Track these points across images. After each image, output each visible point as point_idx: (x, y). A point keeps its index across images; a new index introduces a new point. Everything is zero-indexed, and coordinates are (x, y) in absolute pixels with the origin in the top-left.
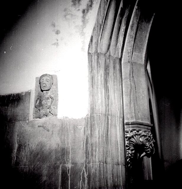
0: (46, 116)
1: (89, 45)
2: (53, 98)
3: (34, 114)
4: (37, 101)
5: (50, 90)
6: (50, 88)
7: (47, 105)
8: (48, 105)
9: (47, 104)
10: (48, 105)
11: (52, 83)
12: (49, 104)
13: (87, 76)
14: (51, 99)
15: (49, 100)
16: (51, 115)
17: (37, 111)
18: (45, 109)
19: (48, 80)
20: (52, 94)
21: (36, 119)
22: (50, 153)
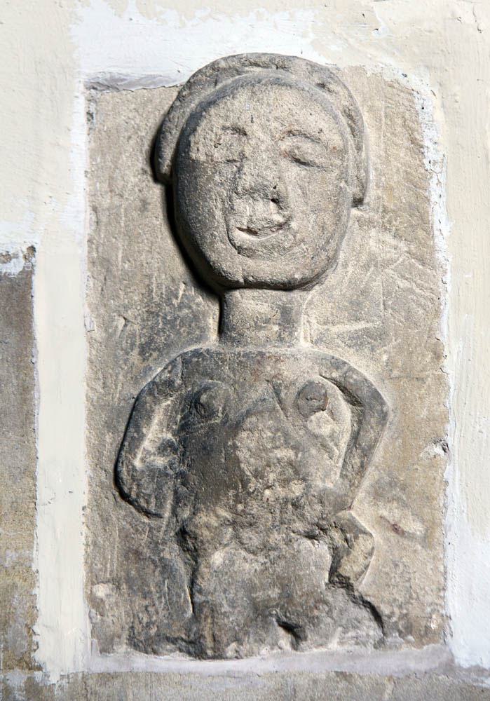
0: (289, 628)
1: (214, 66)
2: (376, 396)
3: (101, 591)
4: (136, 415)
5: (331, 279)
6: (332, 260)
7: (297, 489)
8: (319, 484)
9: (297, 471)
10: (319, 484)
11: (352, 190)
12: (327, 475)
13: (145, 172)
14: (346, 410)
15: (322, 424)
16: (356, 624)
17: (155, 545)
18: (276, 537)
19: (308, 149)
20: (357, 341)
21: (141, 661)
22: (102, 407)
